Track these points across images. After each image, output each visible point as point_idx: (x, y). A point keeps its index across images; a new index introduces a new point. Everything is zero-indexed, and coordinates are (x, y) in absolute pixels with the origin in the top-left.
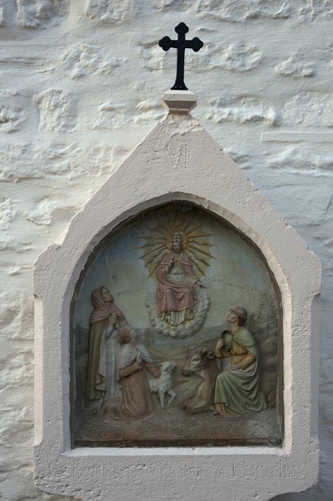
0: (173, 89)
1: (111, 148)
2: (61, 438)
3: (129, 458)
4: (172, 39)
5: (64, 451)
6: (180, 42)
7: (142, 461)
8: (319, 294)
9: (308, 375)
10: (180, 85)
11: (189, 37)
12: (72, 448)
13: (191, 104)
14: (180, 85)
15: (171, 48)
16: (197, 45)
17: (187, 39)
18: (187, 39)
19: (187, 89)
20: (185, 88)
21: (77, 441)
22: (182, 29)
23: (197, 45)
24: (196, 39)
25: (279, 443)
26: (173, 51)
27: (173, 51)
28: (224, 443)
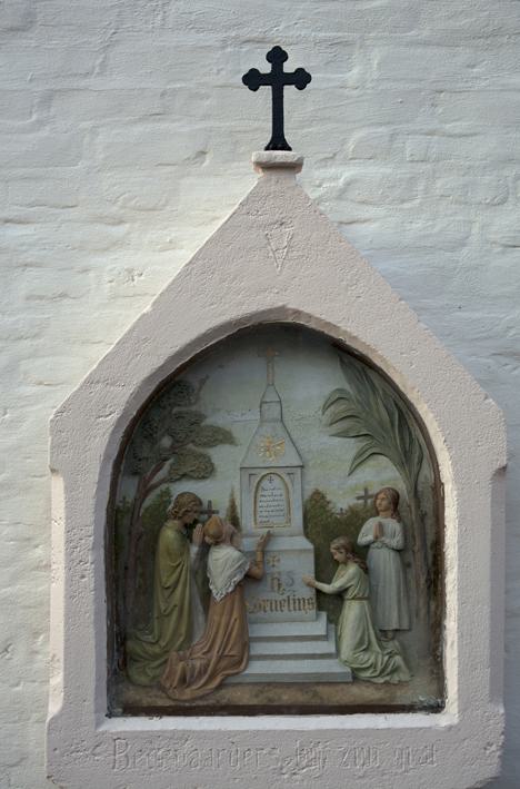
0: (267, 149)
1: (319, 592)
2: (90, 704)
3: (257, 733)
4: (262, 72)
5: (98, 724)
6: (277, 77)
7: (185, 736)
8: (504, 468)
9: (485, 610)
10: (278, 142)
11: (289, 67)
12: (110, 715)
13: (294, 167)
14: (278, 142)
15: (261, 87)
16: (301, 79)
17: (285, 70)
18: (285, 70)
19: (290, 149)
20: (286, 147)
21: (122, 703)
22: (277, 56)
23: (301, 79)
24: (300, 71)
25: (437, 708)
26: (266, 92)
27: (266, 92)
28: (411, 422)
